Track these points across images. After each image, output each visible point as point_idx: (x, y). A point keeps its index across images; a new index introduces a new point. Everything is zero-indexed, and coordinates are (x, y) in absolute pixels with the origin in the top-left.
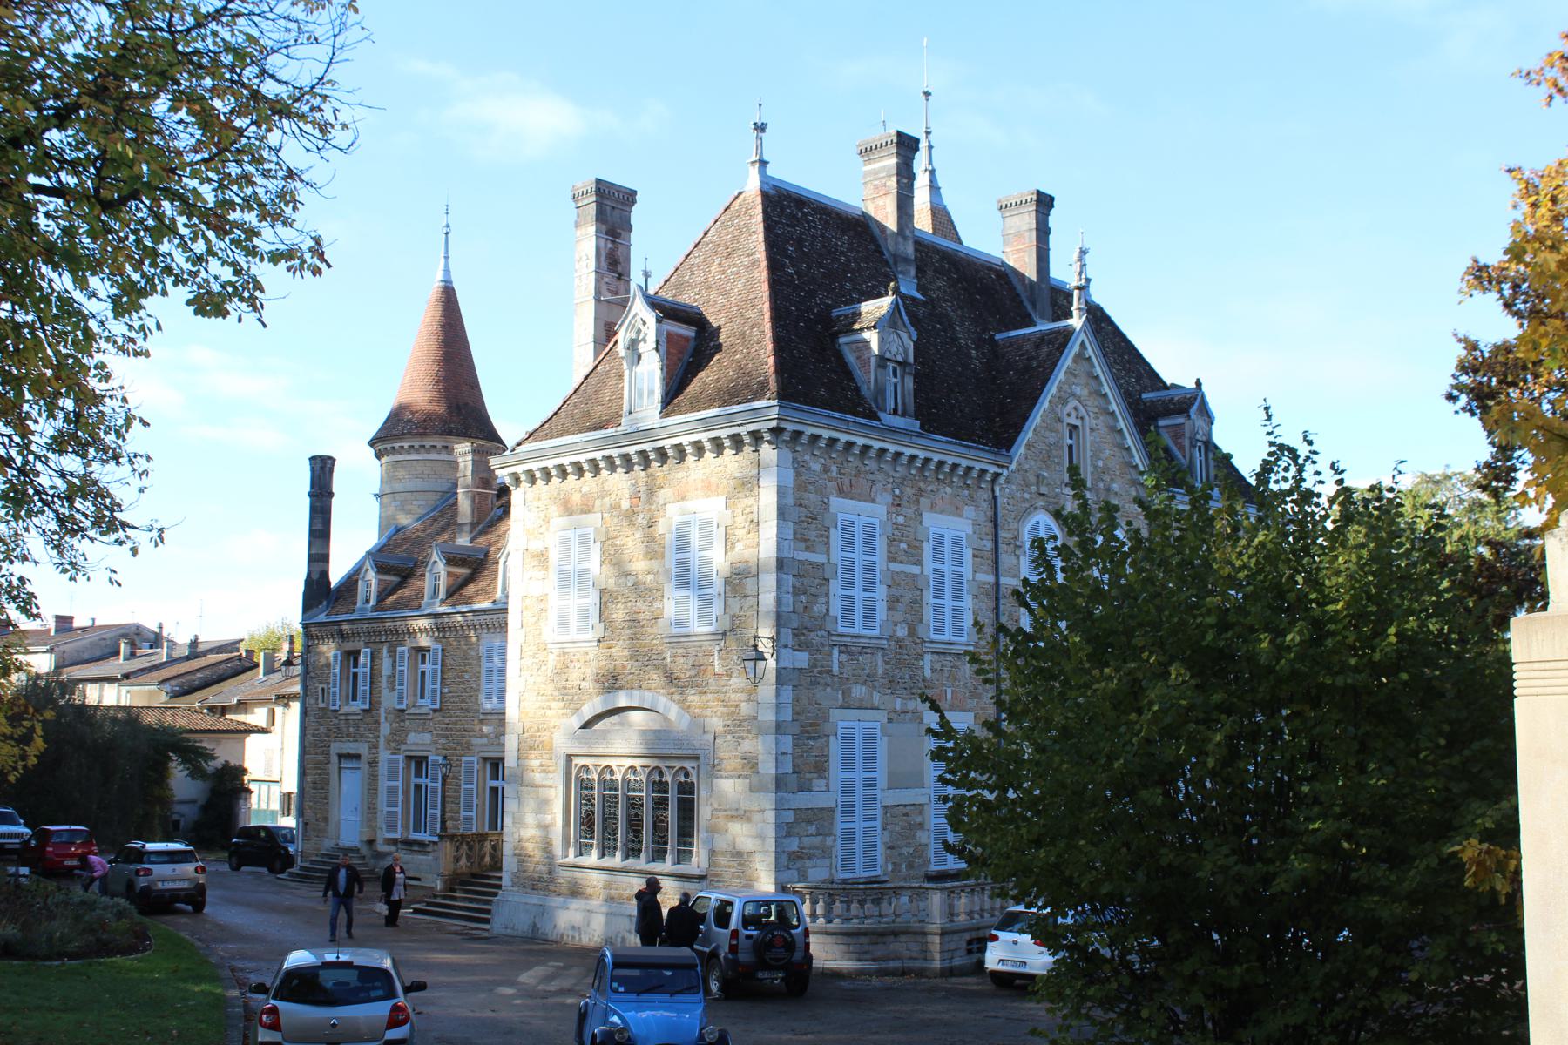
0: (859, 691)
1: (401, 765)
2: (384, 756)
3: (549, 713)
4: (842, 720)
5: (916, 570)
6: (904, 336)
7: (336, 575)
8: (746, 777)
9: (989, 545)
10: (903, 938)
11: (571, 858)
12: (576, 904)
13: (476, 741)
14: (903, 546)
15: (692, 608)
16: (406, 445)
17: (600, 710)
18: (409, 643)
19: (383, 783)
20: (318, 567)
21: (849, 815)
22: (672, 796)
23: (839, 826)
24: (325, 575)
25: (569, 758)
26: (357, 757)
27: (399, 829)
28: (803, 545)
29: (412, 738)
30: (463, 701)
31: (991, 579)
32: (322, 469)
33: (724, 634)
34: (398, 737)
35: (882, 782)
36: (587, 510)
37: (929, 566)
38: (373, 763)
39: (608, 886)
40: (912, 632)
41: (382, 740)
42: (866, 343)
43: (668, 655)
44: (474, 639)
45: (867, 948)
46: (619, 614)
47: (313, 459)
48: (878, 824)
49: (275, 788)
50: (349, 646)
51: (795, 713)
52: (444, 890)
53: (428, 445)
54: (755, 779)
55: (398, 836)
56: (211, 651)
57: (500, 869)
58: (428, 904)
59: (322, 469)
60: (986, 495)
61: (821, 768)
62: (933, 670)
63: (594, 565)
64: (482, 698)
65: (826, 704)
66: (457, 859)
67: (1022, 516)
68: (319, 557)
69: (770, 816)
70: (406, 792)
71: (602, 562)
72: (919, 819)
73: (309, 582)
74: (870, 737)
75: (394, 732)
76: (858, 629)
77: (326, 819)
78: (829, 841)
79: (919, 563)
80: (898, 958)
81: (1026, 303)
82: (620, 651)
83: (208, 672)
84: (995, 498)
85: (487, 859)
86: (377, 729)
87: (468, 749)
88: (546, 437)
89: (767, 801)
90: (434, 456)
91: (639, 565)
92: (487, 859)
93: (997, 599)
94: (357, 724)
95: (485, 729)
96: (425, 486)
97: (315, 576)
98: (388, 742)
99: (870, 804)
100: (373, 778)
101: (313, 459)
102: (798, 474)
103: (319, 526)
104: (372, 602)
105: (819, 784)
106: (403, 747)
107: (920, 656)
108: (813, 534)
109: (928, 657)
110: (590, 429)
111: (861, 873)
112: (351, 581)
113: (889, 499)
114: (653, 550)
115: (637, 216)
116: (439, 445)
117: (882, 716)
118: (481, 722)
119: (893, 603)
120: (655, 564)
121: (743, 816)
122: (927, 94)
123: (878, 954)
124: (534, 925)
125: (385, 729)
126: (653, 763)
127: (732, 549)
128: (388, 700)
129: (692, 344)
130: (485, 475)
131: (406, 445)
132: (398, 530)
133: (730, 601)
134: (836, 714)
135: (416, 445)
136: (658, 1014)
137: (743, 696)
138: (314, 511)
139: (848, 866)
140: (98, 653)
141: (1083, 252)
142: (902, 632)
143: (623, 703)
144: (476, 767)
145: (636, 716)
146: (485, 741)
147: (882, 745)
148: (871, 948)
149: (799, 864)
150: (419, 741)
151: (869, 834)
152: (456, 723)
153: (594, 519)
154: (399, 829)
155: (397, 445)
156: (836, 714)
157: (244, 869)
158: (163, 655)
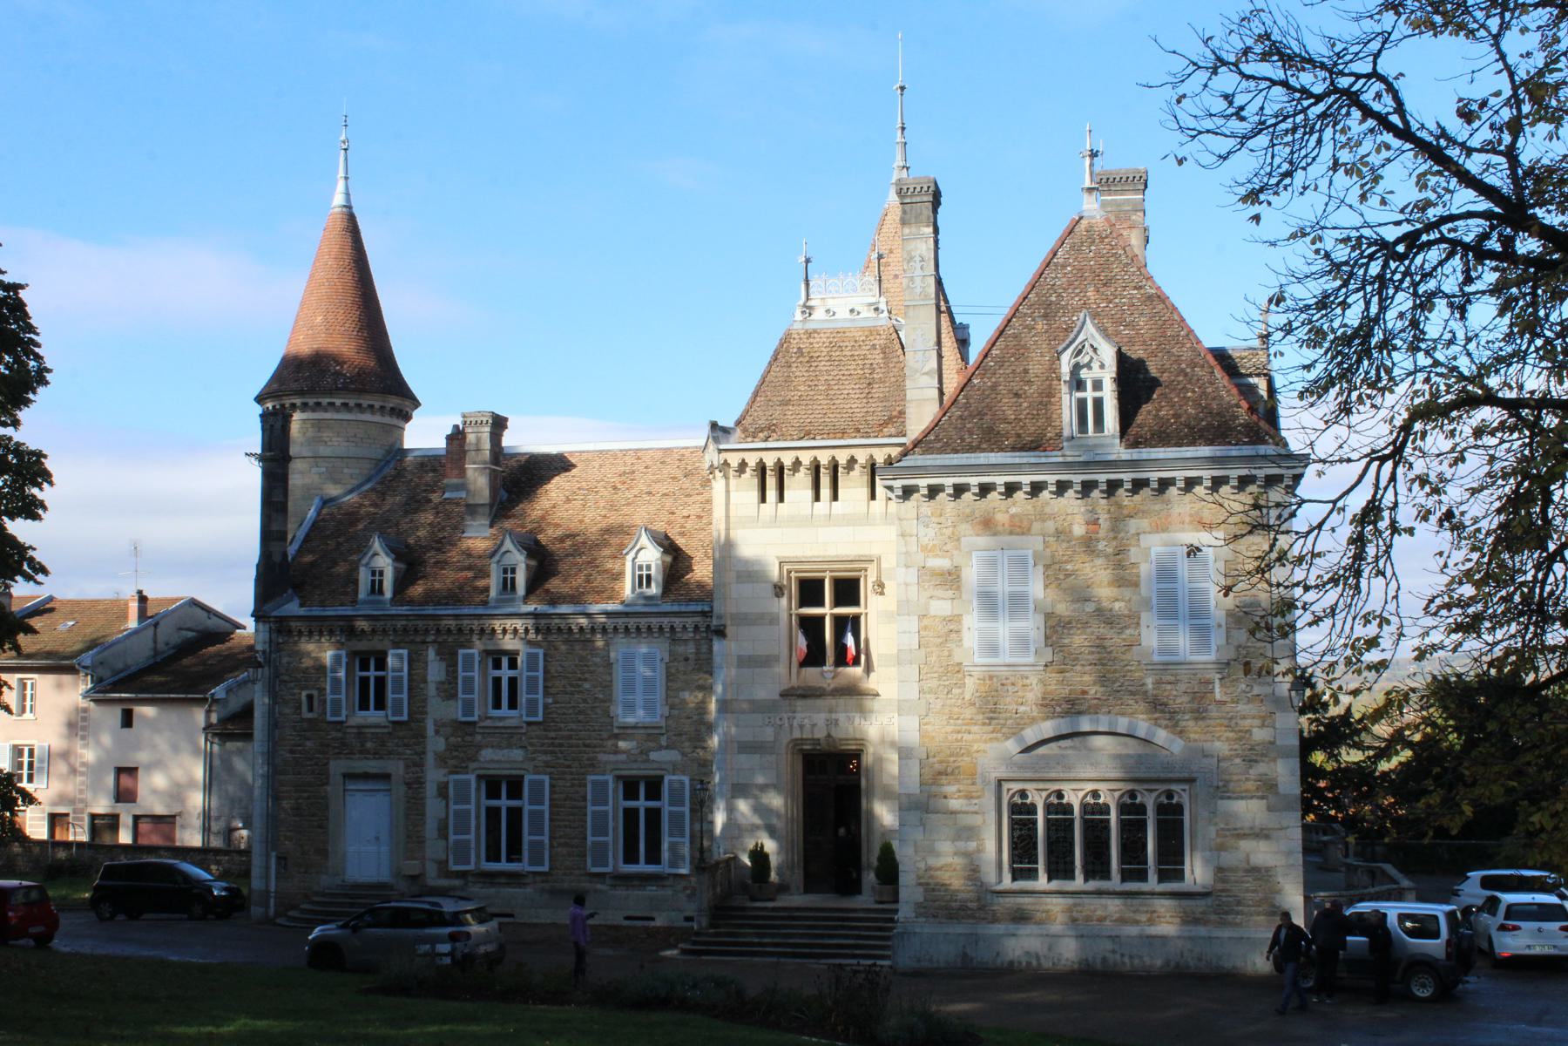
8: (1262, 798)
11: (1007, 882)
12: (1025, 930)
13: (603, 757)
15: (1183, 642)
16: (338, 402)
17: (1064, 732)
18: (478, 646)
25: (1000, 782)
26: (386, 777)
30: (580, 712)
33: (1228, 664)
36: (1026, 532)
39: (1069, 910)
41: (430, 759)
44: (600, 644)
46: (1078, 640)
52: (712, 926)
53: (365, 403)
54: (1273, 799)
55: (471, 867)
57: (897, 901)
58: (695, 943)
63: (1036, 588)
69: (1297, 834)
71: (1046, 586)
82: (1084, 679)
87: (593, 765)
90: (367, 417)
91: (1105, 592)
95: (622, 744)
104: (388, 594)
106: (472, 765)
110: (1014, 449)
114: (1124, 578)
116: (377, 405)
120: (1127, 593)
121: (1262, 834)
124: (965, 955)
126: (1129, 786)
128: (439, 710)
131: (338, 402)
133: (1234, 632)
135: (352, 403)
137: (1257, 722)
141: (808, 261)
143: (1086, 727)
144: (611, 786)
145: (1099, 741)
146: (623, 757)
152: (570, 737)
153: (1036, 543)
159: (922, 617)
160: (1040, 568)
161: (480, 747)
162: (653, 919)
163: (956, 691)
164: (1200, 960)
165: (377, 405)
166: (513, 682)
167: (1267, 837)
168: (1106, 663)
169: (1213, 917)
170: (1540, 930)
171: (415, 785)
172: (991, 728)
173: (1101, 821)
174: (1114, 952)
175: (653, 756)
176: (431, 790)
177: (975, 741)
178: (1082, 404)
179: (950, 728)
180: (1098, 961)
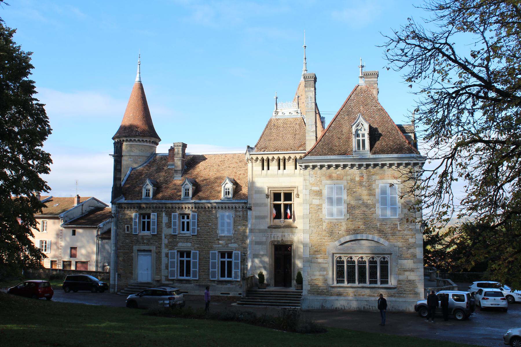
11: (335, 284)
17: (353, 239)
27: (176, 276)
29: (180, 244)
38: (159, 253)
41: (163, 246)
42: (410, 136)
43: (378, 224)
50: (143, 212)
52: (247, 296)
53: (145, 140)
54: (415, 260)
55: (175, 278)
58: (241, 301)
63: (344, 196)
64: (219, 232)
71: (347, 196)
77: (132, 273)
88: (312, 155)
89: (421, 266)
90: (145, 144)
94: (149, 240)
96: (143, 154)
100: (158, 259)
116: (148, 140)
118: (219, 240)
122: (305, 47)
128: (166, 231)
131: (137, 139)
132: (133, 169)
133: (404, 210)
135: (141, 140)
136: (93, 325)
143: (359, 238)
144: (217, 254)
146: (221, 246)
152: (205, 240)
154: (176, 276)
155: (133, 139)
157: (79, 291)
160: (346, 190)
161: (178, 242)
167: (413, 271)
169: (397, 295)
174: (367, 305)
175: (230, 245)
176: (163, 255)
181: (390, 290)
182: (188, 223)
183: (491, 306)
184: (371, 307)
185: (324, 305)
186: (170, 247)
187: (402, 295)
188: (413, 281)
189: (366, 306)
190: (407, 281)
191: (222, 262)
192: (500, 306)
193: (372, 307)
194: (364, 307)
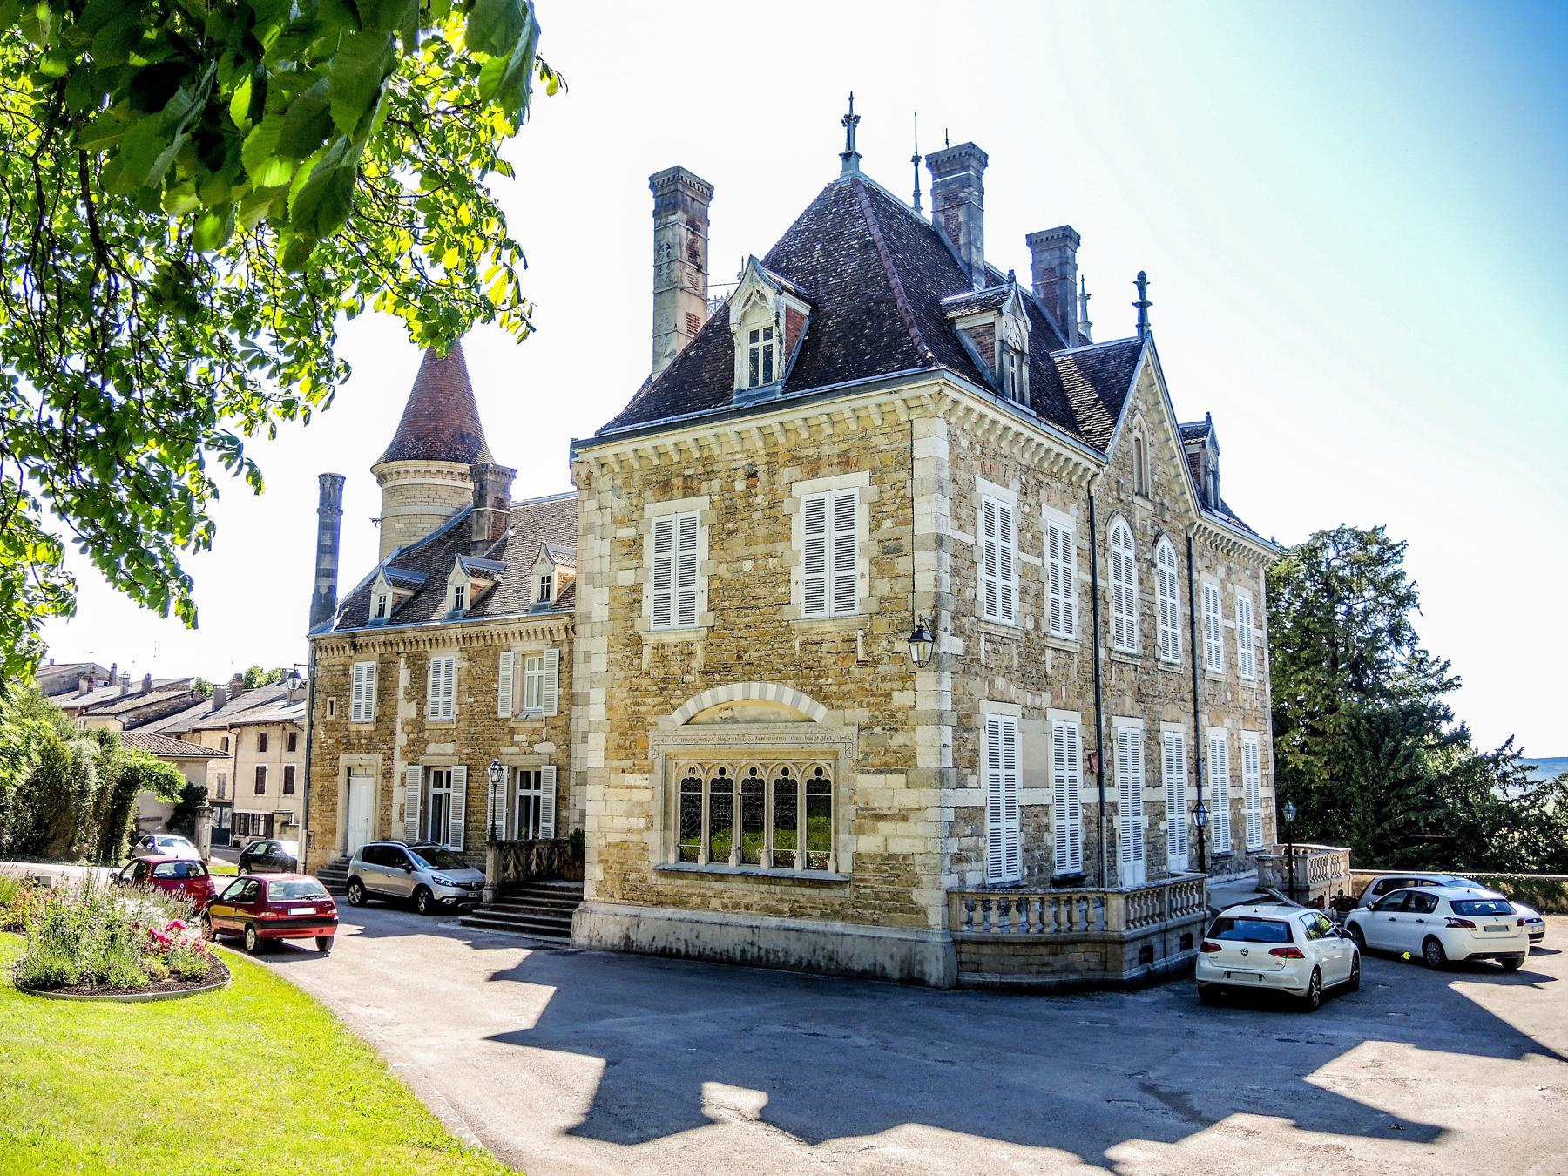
0: (1000, 683)
1: (420, 775)
2: (400, 766)
3: (643, 709)
4: (990, 712)
5: (1037, 561)
6: (1021, 324)
7: (345, 588)
9: (1087, 545)
10: (1080, 948)
14: (1029, 536)
19: (398, 795)
20: (326, 582)
21: (996, 817)
22: (769, 795)
23: (989, 826)
24: (332, 589)
28: (956, 523)
29: (431, 748)
31: (1089, 579)
32: (331, 487)
34: (416, 747)
35: (1019, 782)
37: (1048, 560)
40: (1037, 627)
45: (1047, 959)
47: (323, 477)
48: (1016, 825)
49: (227, 809)
51: (955, 703)
52: (494, 901)
56: (158, 689)
58: (478, 916)
59: (331, 487)
60: (1084, 495)
61: (973, 765)
62: (1053, 667)
65: (977, 695)
66: (506, 868)
67: (1107, 521)
68: (326, 573)
70: (424, 803)
72: (1045, 821)
73: (317, 594)
74: (1009, 728)
75: (411, 743)
76: (998, 618)
78: (981, 840)
79: (1040, 555)
80: (1075, 971)
81: (1058, 332)
83: (162, 706)
84: (1091, 498)
85: (533, 867)
86: (393, 740)
90: (438, 481)
92: (533, 867)
93: (1095, 599)
97: (324, 591)
98: (404, 753)
99: (1010, 804)
101: (323, 477)
102: (952, 448)
103: (328, 542)
104: (388, 614)
105: (972, 781)
106: (422, 758)
107: (1042, 653)
108: (964, 514)
109: (1048, 652)
111: (1006, 878)
112: (362, 597)
113: (1019, 486)
115: (715, 210)
116: (422, 469)
117: (1016, 710)
119: (1024, 592)
123: (1058, 966)
125: (401, 740)
127: (878, 526)
129: (806, 323)
130: (500, 495)
133: (878, 583)
134: (985, 706)
138: (323, 526)
139: (996, 874)
140: (57, 689)
142: (1030, 625)
146: (516, 749)
147: (1018, 738)
148: (1050, 959)
149: (959, 868)
150: (440, 752)
151: (1010, 832)
156: (985, 706)
158: (115, 691)
159: (612, 588)
160: (706, 528)
161: (427, 743)
162: (1273, 952)
163: (636, 662)
164: (831, 959)
165: (402, 470)
166: (1059, 767)
167: (905, 819)
168: (59, 509)
169: (851, 911)
170: (1245, 952)
171: (387, 774)
172: (661, 699)
173: (790, 798)
174: (752, 944)
175: (537, 748)
176: (397, 779)
177: (648, 713)
178: (754, 352)
179: (629, 701)
180: (738, 953)
181: (824, 892)
182: (1059, 767)
183: (1225, 980)
184: (763, 953)
185: (633, 937)
186: (410, 756)
187: (867, 913)
188: (905, 857)
189: (748, 948)
190: (884, 858)
191: (525, 800)
192: (1263, 984)
193: (767, 951)
194: (743, 951)
